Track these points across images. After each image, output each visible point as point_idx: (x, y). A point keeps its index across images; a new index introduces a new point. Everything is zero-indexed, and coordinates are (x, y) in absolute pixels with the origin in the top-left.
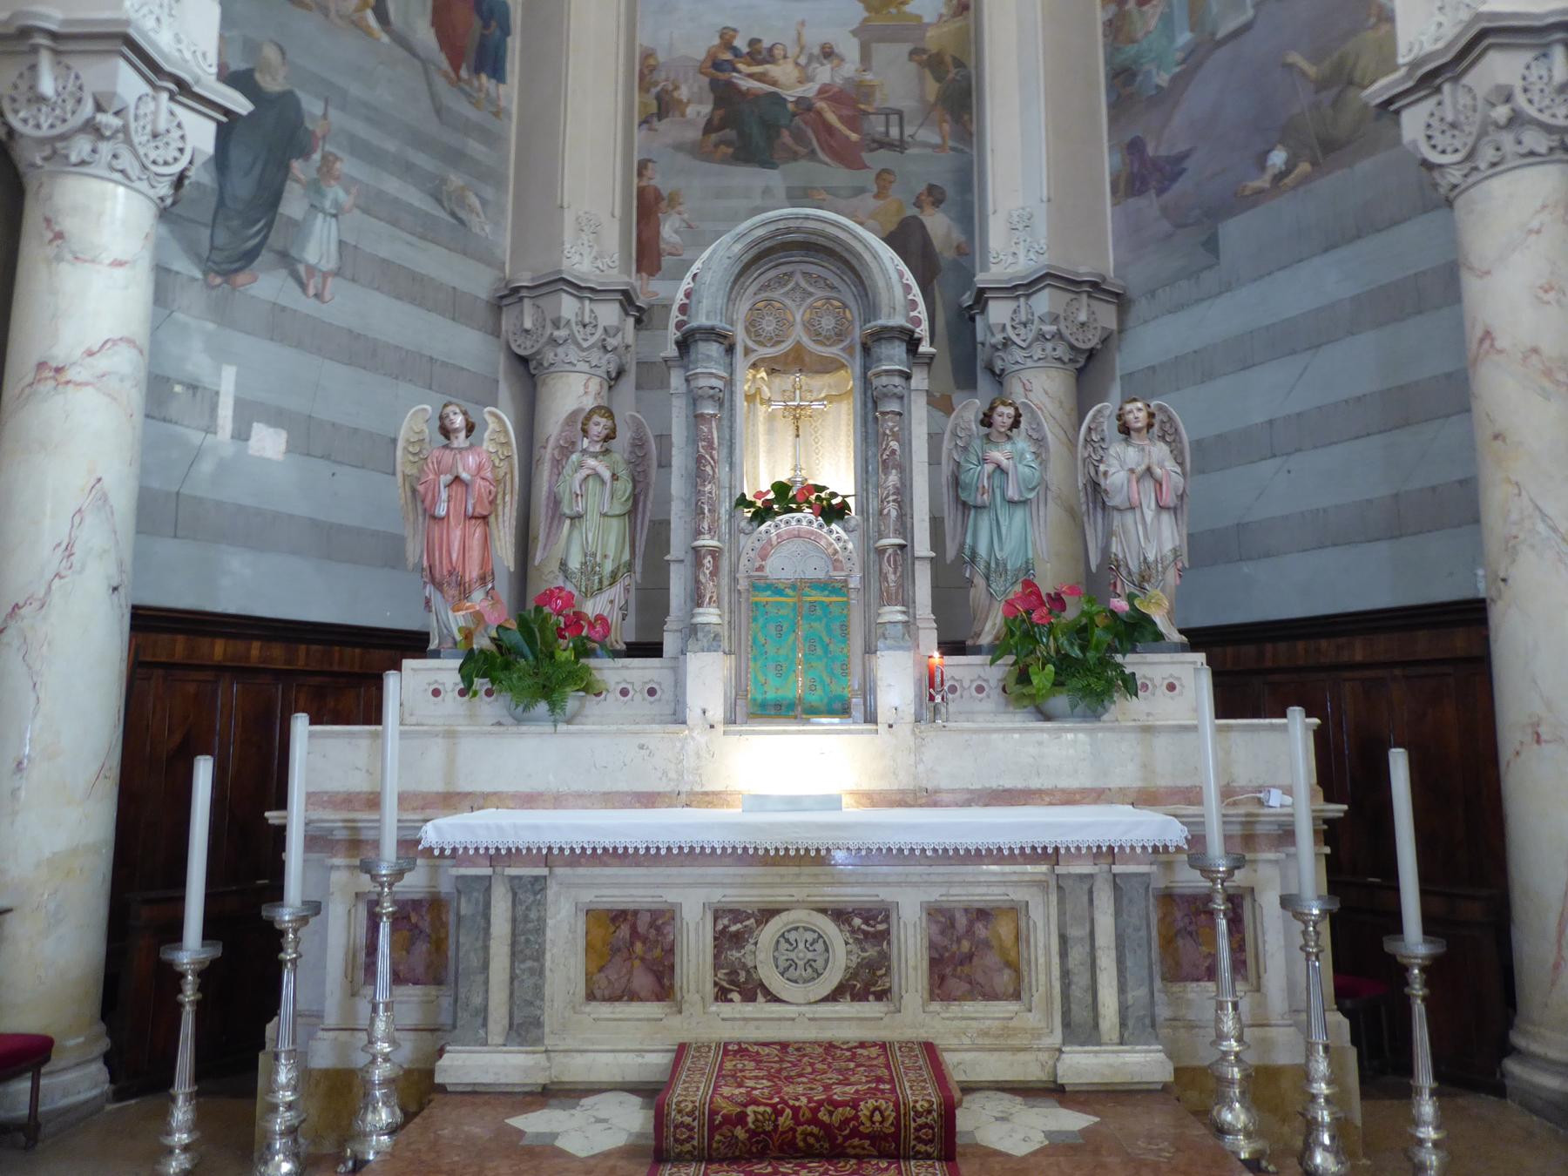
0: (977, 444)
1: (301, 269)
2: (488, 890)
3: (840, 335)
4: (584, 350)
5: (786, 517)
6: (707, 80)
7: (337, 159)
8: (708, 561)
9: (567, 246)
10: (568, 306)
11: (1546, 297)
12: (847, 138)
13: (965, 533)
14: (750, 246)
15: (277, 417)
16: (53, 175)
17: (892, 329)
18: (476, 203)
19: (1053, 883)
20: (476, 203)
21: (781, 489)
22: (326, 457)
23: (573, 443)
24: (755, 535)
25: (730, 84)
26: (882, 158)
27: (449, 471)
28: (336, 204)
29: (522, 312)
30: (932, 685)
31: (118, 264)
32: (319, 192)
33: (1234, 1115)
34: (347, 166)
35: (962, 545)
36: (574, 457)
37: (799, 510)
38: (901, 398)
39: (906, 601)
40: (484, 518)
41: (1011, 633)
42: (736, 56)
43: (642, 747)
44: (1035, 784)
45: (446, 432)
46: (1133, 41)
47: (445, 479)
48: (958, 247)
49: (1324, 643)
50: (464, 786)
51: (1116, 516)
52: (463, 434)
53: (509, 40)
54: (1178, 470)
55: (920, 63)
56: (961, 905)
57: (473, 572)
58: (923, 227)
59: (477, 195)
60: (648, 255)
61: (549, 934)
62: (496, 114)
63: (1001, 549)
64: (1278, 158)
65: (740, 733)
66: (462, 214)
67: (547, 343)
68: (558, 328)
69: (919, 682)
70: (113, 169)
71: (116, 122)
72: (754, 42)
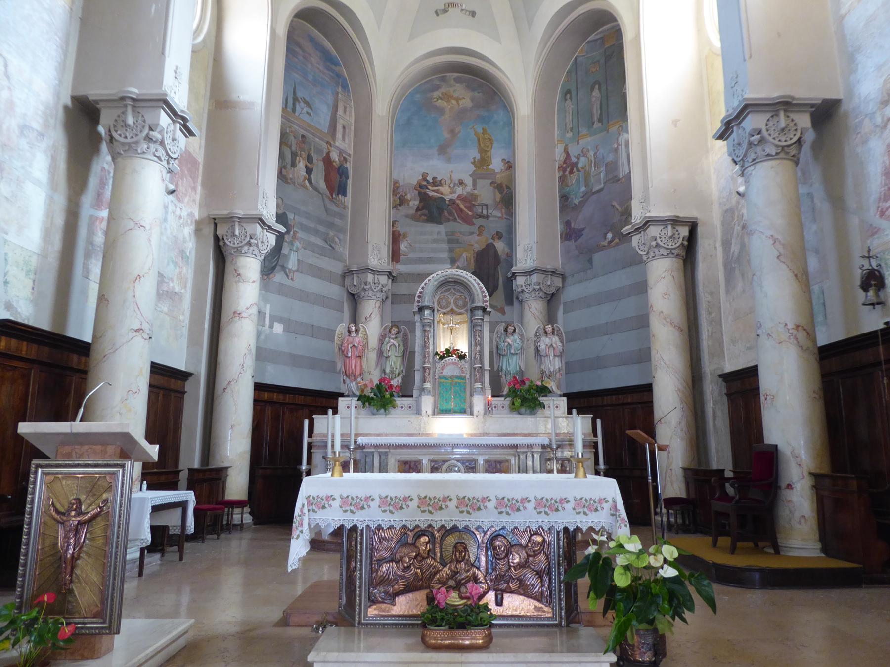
1: (287, 270)
2: (373, 455)
3: (464, 306)
4: (374, 292)
5: (449, 358)
8: (427, 370)
9: (369, 256)
10: (370, 277)
11: (665, 297)
12: (468, 214)
14: (438, 283)
15: (281, 320)
16: (236, 257)
18: (337, 240)
19: (517, 454)
20: (337, 240)
21: (447, 350)
22: (294, 332)
24: (440, 363)
25: (425, 193)
26: (479, 222)
27: (351, 343)
28: (297, 248)
29: (353, 279)
30: (488, 405)
31: (254, 282)
32: (293, 245)
33: (601, 562)
34: (300, 234)
35: (499, 367)
36: (387, 339)
37: (452, 356)
38: (481, 326)
39: (482, 382)
40: (360, 357)
41: (510, 391)
42: (428, 183)
44: (516, 432)
46: (568, 186)
47: (350, 345)
48: (507, 254)
49: (620, 396)
50: (359, 432)
52: (354, 333)
54: (561, 345)
55: (494, 187)
57: (358, 373)
59: (338, 238)
60: (395, 256)
63: (509, 367)
64: (610, 236)
66: (333, 245)
68: (366, 285)
69: (485, 405)
70: (252, 254)
71: (255, 241)
72: (434, 178)
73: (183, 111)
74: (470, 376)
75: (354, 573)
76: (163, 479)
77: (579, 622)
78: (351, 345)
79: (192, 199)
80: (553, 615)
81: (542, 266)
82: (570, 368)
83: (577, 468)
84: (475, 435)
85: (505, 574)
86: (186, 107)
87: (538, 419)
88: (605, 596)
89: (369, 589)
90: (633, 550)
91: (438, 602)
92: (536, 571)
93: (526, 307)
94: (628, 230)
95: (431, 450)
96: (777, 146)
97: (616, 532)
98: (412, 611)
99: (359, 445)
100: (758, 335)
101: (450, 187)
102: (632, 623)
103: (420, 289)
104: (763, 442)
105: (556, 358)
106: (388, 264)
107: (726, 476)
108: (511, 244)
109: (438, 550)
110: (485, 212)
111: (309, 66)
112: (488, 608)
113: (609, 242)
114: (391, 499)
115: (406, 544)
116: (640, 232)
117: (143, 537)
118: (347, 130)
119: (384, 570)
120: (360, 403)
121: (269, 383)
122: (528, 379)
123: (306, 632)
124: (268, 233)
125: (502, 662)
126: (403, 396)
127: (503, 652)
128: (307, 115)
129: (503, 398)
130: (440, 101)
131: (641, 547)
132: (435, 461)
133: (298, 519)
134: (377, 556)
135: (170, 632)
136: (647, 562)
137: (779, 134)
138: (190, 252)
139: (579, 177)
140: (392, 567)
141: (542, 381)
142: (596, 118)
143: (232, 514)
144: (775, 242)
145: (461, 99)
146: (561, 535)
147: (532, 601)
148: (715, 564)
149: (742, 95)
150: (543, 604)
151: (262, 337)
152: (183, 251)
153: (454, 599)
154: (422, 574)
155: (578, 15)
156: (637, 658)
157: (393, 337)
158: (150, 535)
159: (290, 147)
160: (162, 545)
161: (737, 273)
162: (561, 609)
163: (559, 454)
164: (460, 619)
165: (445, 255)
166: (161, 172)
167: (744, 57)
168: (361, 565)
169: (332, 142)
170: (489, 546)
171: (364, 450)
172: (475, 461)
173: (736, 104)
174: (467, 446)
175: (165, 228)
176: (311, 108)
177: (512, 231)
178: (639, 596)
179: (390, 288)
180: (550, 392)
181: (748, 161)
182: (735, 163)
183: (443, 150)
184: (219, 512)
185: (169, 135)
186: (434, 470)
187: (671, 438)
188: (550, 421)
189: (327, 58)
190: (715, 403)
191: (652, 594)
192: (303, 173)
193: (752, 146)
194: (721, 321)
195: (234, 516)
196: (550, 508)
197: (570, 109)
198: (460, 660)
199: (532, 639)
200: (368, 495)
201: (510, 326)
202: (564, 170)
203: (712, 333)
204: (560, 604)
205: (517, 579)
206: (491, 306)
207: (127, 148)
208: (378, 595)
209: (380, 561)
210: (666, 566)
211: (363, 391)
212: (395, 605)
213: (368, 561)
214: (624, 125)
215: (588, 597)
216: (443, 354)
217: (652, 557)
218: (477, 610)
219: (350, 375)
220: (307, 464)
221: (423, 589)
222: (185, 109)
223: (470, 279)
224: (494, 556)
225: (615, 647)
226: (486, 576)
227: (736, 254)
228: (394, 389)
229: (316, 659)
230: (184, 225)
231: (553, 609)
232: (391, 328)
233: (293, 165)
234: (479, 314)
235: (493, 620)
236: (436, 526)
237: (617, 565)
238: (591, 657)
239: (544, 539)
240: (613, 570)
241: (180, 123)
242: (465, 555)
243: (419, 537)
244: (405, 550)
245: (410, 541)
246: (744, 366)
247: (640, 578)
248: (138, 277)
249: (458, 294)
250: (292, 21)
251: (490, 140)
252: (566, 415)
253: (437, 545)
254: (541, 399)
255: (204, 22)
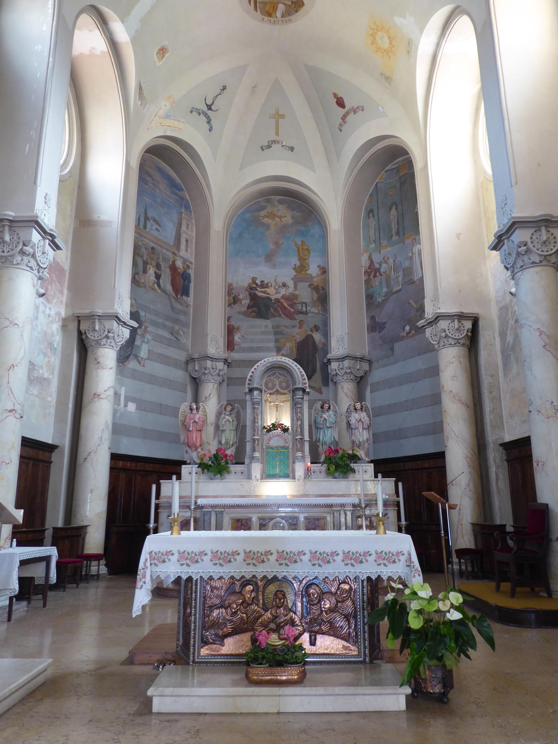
0: (320, 413)
1: (139, 358)
2: (211, 515)
3: (287, 387)
4: (213, 376)
5: (274, 431)
6: (248, 293)
7: (148, 327)
8: (256, 442)
9: (209, 346)
10: (209, 363)
13: (317, 434)
15: (134, 400)
16: (97, 348)
17: (299, 388)
18: (181, 333)
19: (332, 512)
20: (181, 333)
21: (273, 424)
22: (144, 410)
23: (222, 412)
24: (267, 436)
25: (255, 294)
26: (300, 317)
28: (148, 339)
30: (308, 470)
31: (111, 368)
32: (144, 337)
33: (398, 607)
34: (151, 329)
35: (316, 438)
36: (223, 416)
37: (277, 429)
40: (200, 431)
41: (326, 458)
43: (241, 485)
45: (191, 409)
47: (192, 421)
49: (419, 462)
50: (200, 494)
51: (353, 430)
52: (195, 410)
53: (190, 284)
54: (368, 419)
56: (313, 517)
57: (198, 444)
58: (313, 337)
59: (182, 331)
60: (230, 345)
61: (224, 523)
62: (187, 307)
63: (325, 438)
64: (407, 328)
65: (264, 482)
66: (178, 337)
67: (202, 374)
68: (206, 370)
69: (305, 470)
71: (112, 335)
72: (262, 282)
73: (51, 230)
74: (292, 446)
75: (189, 617)
76: (30, 536)
77: (382, 659)
78: (193, 421)
79: (59, 300)
80: (359, 653)
81: (352, 353)
82: (376, 438)
83: (378, 525)
84: (297, 496)
85: (318, 618)
86: (54, 226)
87: (350, 482)
88: (401, 637)
89: (202, 632)
90: (425, 597)
91: (260, 643)
92: (344, 615)
93: (340, 388)
94: (422, 323)
95: (259, 509)
96: (540, 255)
97: (411, 580)
98: (238, 650)
99: (199, 505)
100: (530, 411)
101: (275, 288)
102: (424, 660)
103: (250, 374)
104: (537, 501)
105: (365, 431)
106: (224, 353)
107: (507, 530)
108: (326, 335)
109: (261, 597)
110: (304, 309)
111: (158, 191)
112: (302, 647)
113: (407, 333)
114: (221, 553)
115: (234, 593)
116: (432, 326)
117: (12, 587)
118: (189, 243)
119: (215, 615)
120: (200, 469)
121: (123, 453)
122: (341, 449)
123: (148, 669)
124: (123, 328)
125: (315, 695)
126: (236, 463)
127: (316, 686)
128: (156, 231)
129: (320, 465)
130: (266, 219)
131: (431, 594)
132: (264, 519)
133: (142, 571)
134: (209, 602)
135: (31, 670)
136: (437, 607)
137: (542, 246)
138: (57, 344)
139: (382, 279)
140: (222, 613)
141: (353, 450)
142: (394, 232)
143: (90, 566)
144: (541, 334)
145: (283, 217)
146: (365, 583)
147: (340, 641)
148: (497, 607)
149: (510, 214)
150: (350, 644)
151: (118, 414)
152: (51, 343)
153: (274, 640)
154: (247, 618)
155: (376, 150)
156: (429, 690)
157: (228, 413)
158: (17, 586)
159: (142, 257)
160: (29, 593)
161: (512, 358)
162: (365, 648)
163: (367, 512)
164: (278, 658)
165: (272, 345)
166: (33, 279)
167: (511, 184)
168: (195, 611)
169: (177, 253)
170: (304, 593)
171: (203, 510)
172: (297, 518)
173: (506, 221)
174: (290, 506)
175: (37, 325)
176: (160, 226)
177: (327, 324)
178: (429, 636)
179: (226, 372)
180: (360, 459)
181: (517, 267)
182: (507, 269)
183: (269, 258)
184: (78, 564)
185: (39, 249)
186: (262, 527)
187: (461, 497)
188: (359, 483)
189: (173, 184)
190: (497, 467)
191: (440, 634)
192: (153, 278)
193: (520, 255)
194: (500, 399)
195: (92, 568)
196: (355, 560)
197: (373, 224)
198: (278, 693)
199: (341, 674)
200: (202, 551)
201: (326, 404)
202: (369, 275)
203: (493, 409)
204: (365, 644)
205: (328, 621)
206: (310, 387)
207: (4, 260)
208: (209, 637)
209: (212, 608)
210: (452, 610)
211: (202, 459)
212: (223, 646)
213: (201, 607)
214: (417, 237)
215: (387, 637)
216: (270, 428)
217: (441, 602)
218: (293, 650)
219: (191, 446)
220: (155, 523)
221: (247, 632)
222: (54, 228)
223: (292, 364)
224: (308, 602)
225: (411, 680)
226: (301, 620)
227: (511, 343)
228: (228, 458)
229: (154, 694)
230: (52, 322)
231: (358, 648)
232: (226, 406)
233: (145, 271)
234: (299, 394)
235: (307, 658)
236: (259, 577)
237: (411, 609)
238: (389, 690)
239: (351, 587)
240: (408, 613)
241: (49, 239)
242: (284, 602)
243: (245, 586)
244: (233, 598)
245: (237, 589)
246: (521, 437)
247: (431, 621)
248: (12, 367)
249: (282, 378)
250: (143, 155)
251: (308, 250)
252: (373, 478)
253: (260, 593)
254: (352, 465)
255: (70, 158)
